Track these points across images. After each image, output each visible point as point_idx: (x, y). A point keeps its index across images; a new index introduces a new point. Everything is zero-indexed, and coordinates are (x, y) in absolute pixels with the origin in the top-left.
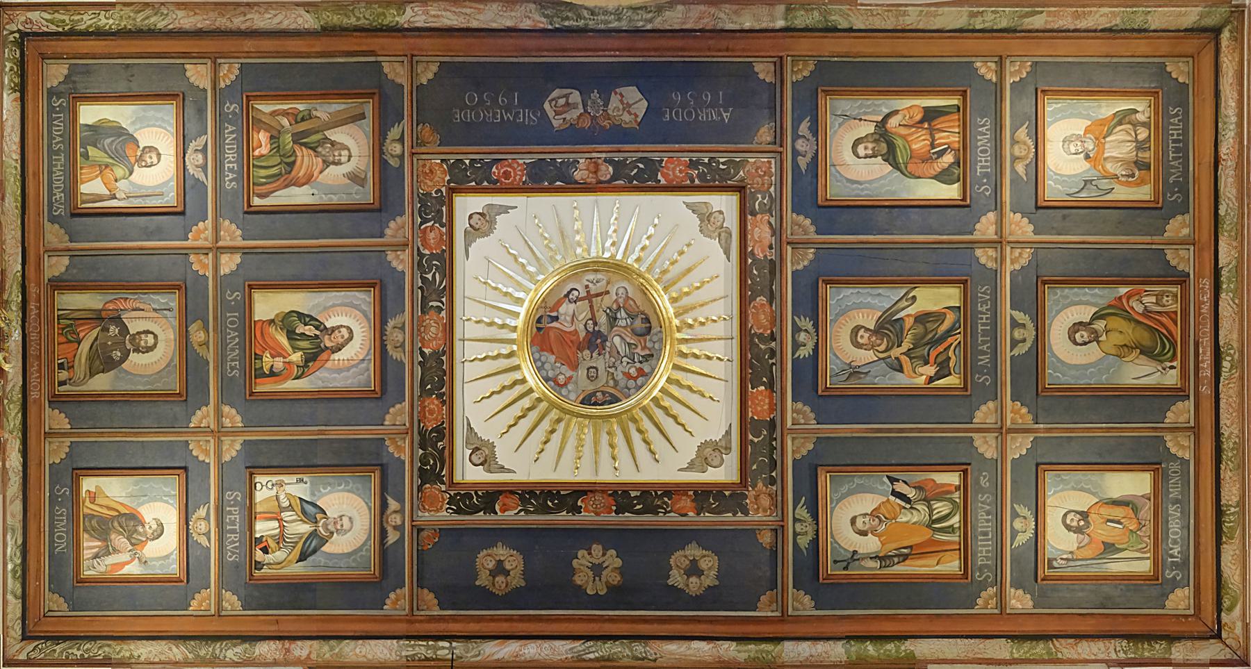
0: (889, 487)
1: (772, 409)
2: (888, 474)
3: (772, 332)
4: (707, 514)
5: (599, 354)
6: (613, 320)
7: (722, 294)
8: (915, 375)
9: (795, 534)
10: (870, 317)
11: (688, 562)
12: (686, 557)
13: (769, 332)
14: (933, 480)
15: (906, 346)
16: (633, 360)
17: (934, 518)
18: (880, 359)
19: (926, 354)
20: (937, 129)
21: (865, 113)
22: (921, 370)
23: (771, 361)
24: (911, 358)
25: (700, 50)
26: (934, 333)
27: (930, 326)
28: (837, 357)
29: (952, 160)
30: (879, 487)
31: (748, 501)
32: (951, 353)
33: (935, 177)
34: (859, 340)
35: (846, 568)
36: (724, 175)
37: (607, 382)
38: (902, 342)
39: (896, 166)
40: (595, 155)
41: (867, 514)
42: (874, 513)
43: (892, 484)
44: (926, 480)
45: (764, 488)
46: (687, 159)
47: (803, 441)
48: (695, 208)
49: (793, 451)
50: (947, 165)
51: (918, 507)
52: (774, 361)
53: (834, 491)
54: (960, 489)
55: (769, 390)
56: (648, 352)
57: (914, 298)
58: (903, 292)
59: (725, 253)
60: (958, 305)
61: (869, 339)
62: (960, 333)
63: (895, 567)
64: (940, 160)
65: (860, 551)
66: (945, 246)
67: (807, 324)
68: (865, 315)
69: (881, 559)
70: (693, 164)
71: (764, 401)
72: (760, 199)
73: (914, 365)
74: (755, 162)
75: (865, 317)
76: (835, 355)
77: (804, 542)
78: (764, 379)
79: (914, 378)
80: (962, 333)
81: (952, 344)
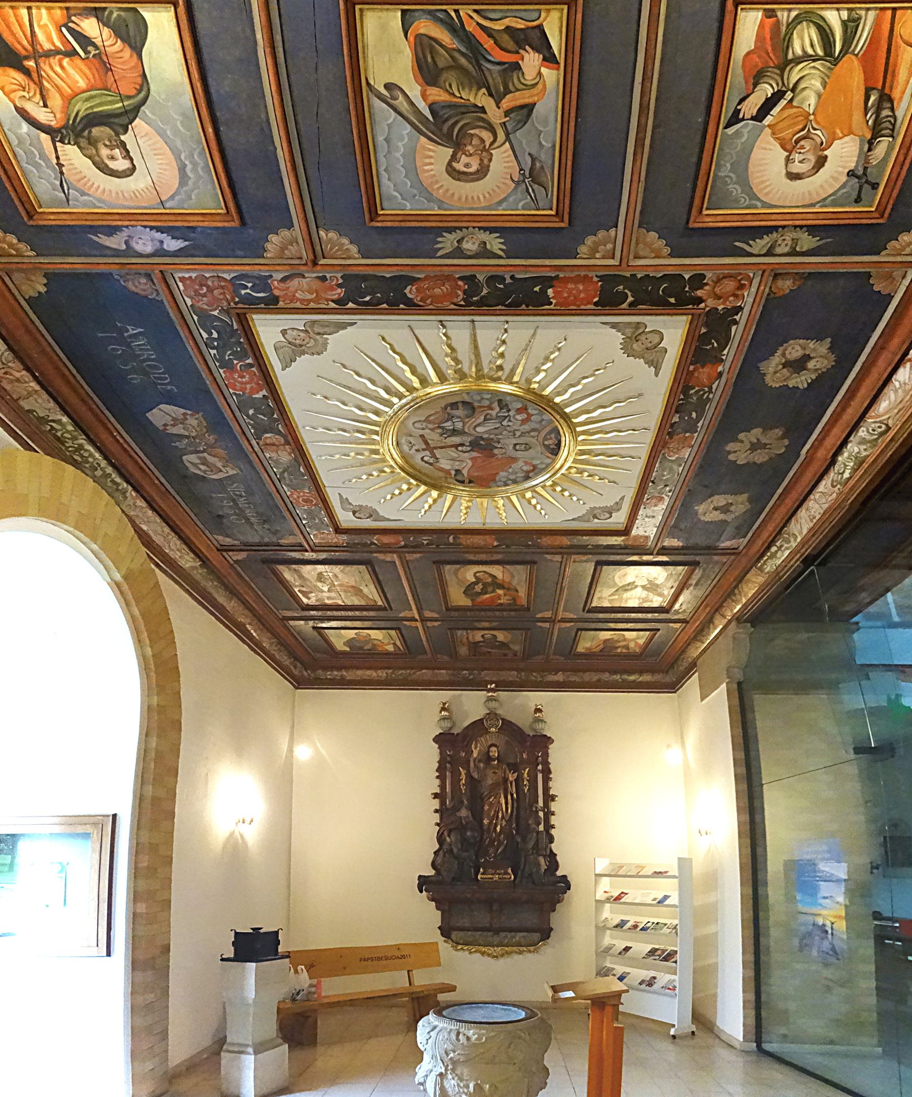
0: (747, 125)
1: (586, 279)
2: (721, 127)
3: (461, 278)
4: (725, 352)
5: (499, 442)
6: (454, 432)
7: (408, 331)
8: (540, 86)
9: (793, 253)
10: (431, 154)
11: (785, 370)
12: (775, 372)
13: (460, 283)
14: (748, 53)
15: (482, 99)
16: (506, 417)
17: (820, 52)
18: (508, 139)
19: (498, 68)
20: (32, 45)
21: (43, 156)
22: (529, 74)
23: (508, 281)
24: (507, 91)
25: (50, 360)
26: (457, 55)
27: (443, 59)
28: (505, 199)
29: (93, 21)
30: (743, 140)
31: (720, 308)
32: (498, 26)
33: (137, 48)
34: (472, 169)
35: (875, 186)
36: (226, 333)
37: (533, 437)
38: (476, 106)
39: (133, 113)
40: (257, 448)
41: (788, 157)
42: (789, 147)
43: (743, 119)
44: (743, 65)
45: (707, 288)
46: (221, 371)
47: (641, 246)
48: (288, 360)
49: (656, 257)
50: (106, 31)
51: (794, 78)
52: (507, 277)
53: (735, 203)
54: (773, 10)
55: (555, 283)
56: (496, 404)
57: (388, 86)
58: (377, 103)
59: (344, 328)
60: (399, 14)
61: (471, 155)
62: (456, 11)
63: (899, 113)
64: (98, 42)
65: (852, 166)
66: (278, 38)
67: (448, 242)
68: (427, 161)
69: (876, 133)
70: (227, 365)
71: (571, 290)
72: (248, 291)
73: (521, 87)
74: (191, 298)
75: (432, 161)
76: (500, 203)
77: (807, 242)
78: (537, 289)
79: (545, 85)
80: (456, 7)
81: (478, 24)
